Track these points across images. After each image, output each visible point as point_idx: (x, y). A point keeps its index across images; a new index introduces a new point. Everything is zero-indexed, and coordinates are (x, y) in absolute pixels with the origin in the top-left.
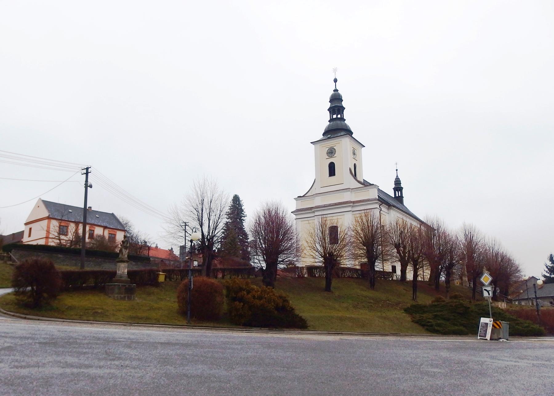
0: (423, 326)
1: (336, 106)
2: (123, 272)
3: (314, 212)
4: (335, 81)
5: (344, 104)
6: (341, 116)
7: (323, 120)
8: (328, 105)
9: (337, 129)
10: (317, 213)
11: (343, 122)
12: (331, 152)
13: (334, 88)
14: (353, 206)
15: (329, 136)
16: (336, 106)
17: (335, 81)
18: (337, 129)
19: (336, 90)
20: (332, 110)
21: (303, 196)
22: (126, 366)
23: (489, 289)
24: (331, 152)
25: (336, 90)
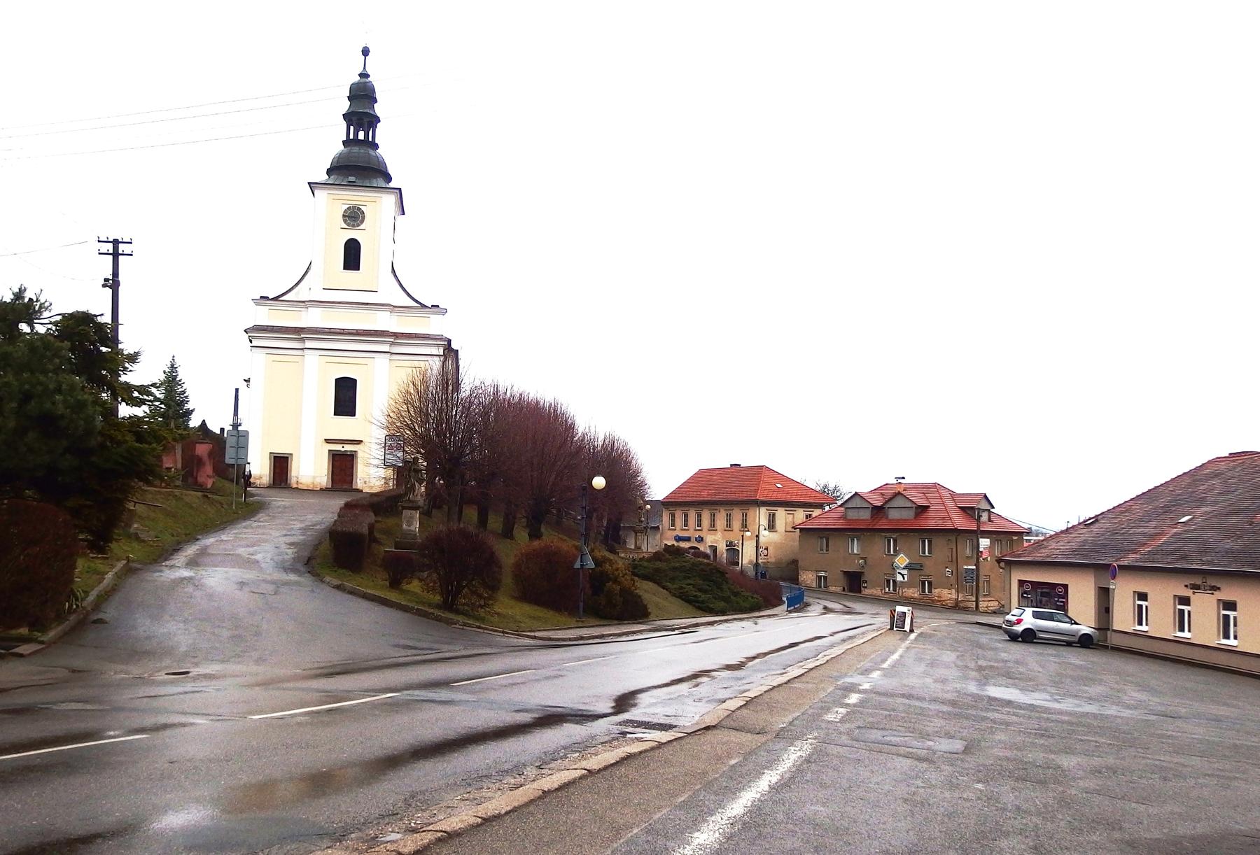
0: (689, 602)
1: (362, 108)
2: (732, 549)
3: (303, 340)
4: (366, 52)
5: (379, 109)
6: (367, 135)
7: (331, 139)
8: (345, 106)
9: (359, 167)
10: (309, 344)
11: (371, 152)
12: (354, 217)
13: (360, 70)
14: (392, 344)
15: (352, 179)
16: (362, 108)
17: (366, 52)
18: (359, 167)
19: (364, 75)
20: (350, 118)
21: (276, 299)
22: (700, 700)
23: (905, 572)
24: (354, 217)
25: (364, 75)
